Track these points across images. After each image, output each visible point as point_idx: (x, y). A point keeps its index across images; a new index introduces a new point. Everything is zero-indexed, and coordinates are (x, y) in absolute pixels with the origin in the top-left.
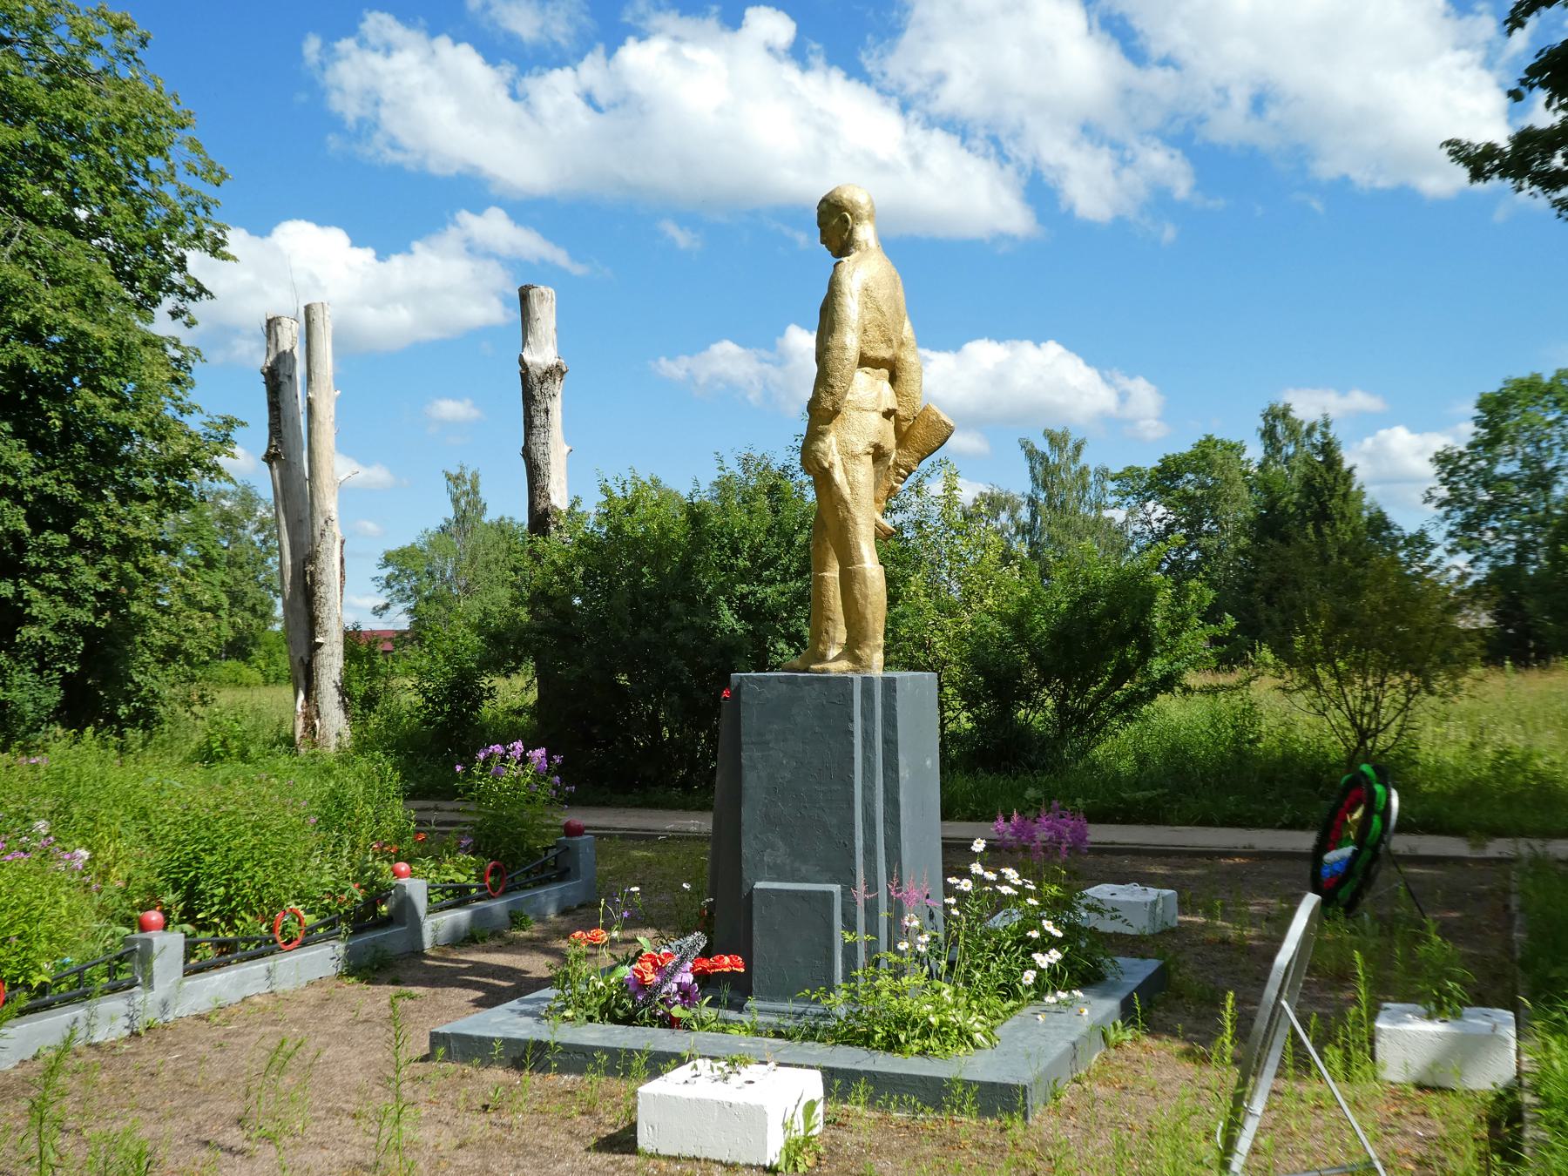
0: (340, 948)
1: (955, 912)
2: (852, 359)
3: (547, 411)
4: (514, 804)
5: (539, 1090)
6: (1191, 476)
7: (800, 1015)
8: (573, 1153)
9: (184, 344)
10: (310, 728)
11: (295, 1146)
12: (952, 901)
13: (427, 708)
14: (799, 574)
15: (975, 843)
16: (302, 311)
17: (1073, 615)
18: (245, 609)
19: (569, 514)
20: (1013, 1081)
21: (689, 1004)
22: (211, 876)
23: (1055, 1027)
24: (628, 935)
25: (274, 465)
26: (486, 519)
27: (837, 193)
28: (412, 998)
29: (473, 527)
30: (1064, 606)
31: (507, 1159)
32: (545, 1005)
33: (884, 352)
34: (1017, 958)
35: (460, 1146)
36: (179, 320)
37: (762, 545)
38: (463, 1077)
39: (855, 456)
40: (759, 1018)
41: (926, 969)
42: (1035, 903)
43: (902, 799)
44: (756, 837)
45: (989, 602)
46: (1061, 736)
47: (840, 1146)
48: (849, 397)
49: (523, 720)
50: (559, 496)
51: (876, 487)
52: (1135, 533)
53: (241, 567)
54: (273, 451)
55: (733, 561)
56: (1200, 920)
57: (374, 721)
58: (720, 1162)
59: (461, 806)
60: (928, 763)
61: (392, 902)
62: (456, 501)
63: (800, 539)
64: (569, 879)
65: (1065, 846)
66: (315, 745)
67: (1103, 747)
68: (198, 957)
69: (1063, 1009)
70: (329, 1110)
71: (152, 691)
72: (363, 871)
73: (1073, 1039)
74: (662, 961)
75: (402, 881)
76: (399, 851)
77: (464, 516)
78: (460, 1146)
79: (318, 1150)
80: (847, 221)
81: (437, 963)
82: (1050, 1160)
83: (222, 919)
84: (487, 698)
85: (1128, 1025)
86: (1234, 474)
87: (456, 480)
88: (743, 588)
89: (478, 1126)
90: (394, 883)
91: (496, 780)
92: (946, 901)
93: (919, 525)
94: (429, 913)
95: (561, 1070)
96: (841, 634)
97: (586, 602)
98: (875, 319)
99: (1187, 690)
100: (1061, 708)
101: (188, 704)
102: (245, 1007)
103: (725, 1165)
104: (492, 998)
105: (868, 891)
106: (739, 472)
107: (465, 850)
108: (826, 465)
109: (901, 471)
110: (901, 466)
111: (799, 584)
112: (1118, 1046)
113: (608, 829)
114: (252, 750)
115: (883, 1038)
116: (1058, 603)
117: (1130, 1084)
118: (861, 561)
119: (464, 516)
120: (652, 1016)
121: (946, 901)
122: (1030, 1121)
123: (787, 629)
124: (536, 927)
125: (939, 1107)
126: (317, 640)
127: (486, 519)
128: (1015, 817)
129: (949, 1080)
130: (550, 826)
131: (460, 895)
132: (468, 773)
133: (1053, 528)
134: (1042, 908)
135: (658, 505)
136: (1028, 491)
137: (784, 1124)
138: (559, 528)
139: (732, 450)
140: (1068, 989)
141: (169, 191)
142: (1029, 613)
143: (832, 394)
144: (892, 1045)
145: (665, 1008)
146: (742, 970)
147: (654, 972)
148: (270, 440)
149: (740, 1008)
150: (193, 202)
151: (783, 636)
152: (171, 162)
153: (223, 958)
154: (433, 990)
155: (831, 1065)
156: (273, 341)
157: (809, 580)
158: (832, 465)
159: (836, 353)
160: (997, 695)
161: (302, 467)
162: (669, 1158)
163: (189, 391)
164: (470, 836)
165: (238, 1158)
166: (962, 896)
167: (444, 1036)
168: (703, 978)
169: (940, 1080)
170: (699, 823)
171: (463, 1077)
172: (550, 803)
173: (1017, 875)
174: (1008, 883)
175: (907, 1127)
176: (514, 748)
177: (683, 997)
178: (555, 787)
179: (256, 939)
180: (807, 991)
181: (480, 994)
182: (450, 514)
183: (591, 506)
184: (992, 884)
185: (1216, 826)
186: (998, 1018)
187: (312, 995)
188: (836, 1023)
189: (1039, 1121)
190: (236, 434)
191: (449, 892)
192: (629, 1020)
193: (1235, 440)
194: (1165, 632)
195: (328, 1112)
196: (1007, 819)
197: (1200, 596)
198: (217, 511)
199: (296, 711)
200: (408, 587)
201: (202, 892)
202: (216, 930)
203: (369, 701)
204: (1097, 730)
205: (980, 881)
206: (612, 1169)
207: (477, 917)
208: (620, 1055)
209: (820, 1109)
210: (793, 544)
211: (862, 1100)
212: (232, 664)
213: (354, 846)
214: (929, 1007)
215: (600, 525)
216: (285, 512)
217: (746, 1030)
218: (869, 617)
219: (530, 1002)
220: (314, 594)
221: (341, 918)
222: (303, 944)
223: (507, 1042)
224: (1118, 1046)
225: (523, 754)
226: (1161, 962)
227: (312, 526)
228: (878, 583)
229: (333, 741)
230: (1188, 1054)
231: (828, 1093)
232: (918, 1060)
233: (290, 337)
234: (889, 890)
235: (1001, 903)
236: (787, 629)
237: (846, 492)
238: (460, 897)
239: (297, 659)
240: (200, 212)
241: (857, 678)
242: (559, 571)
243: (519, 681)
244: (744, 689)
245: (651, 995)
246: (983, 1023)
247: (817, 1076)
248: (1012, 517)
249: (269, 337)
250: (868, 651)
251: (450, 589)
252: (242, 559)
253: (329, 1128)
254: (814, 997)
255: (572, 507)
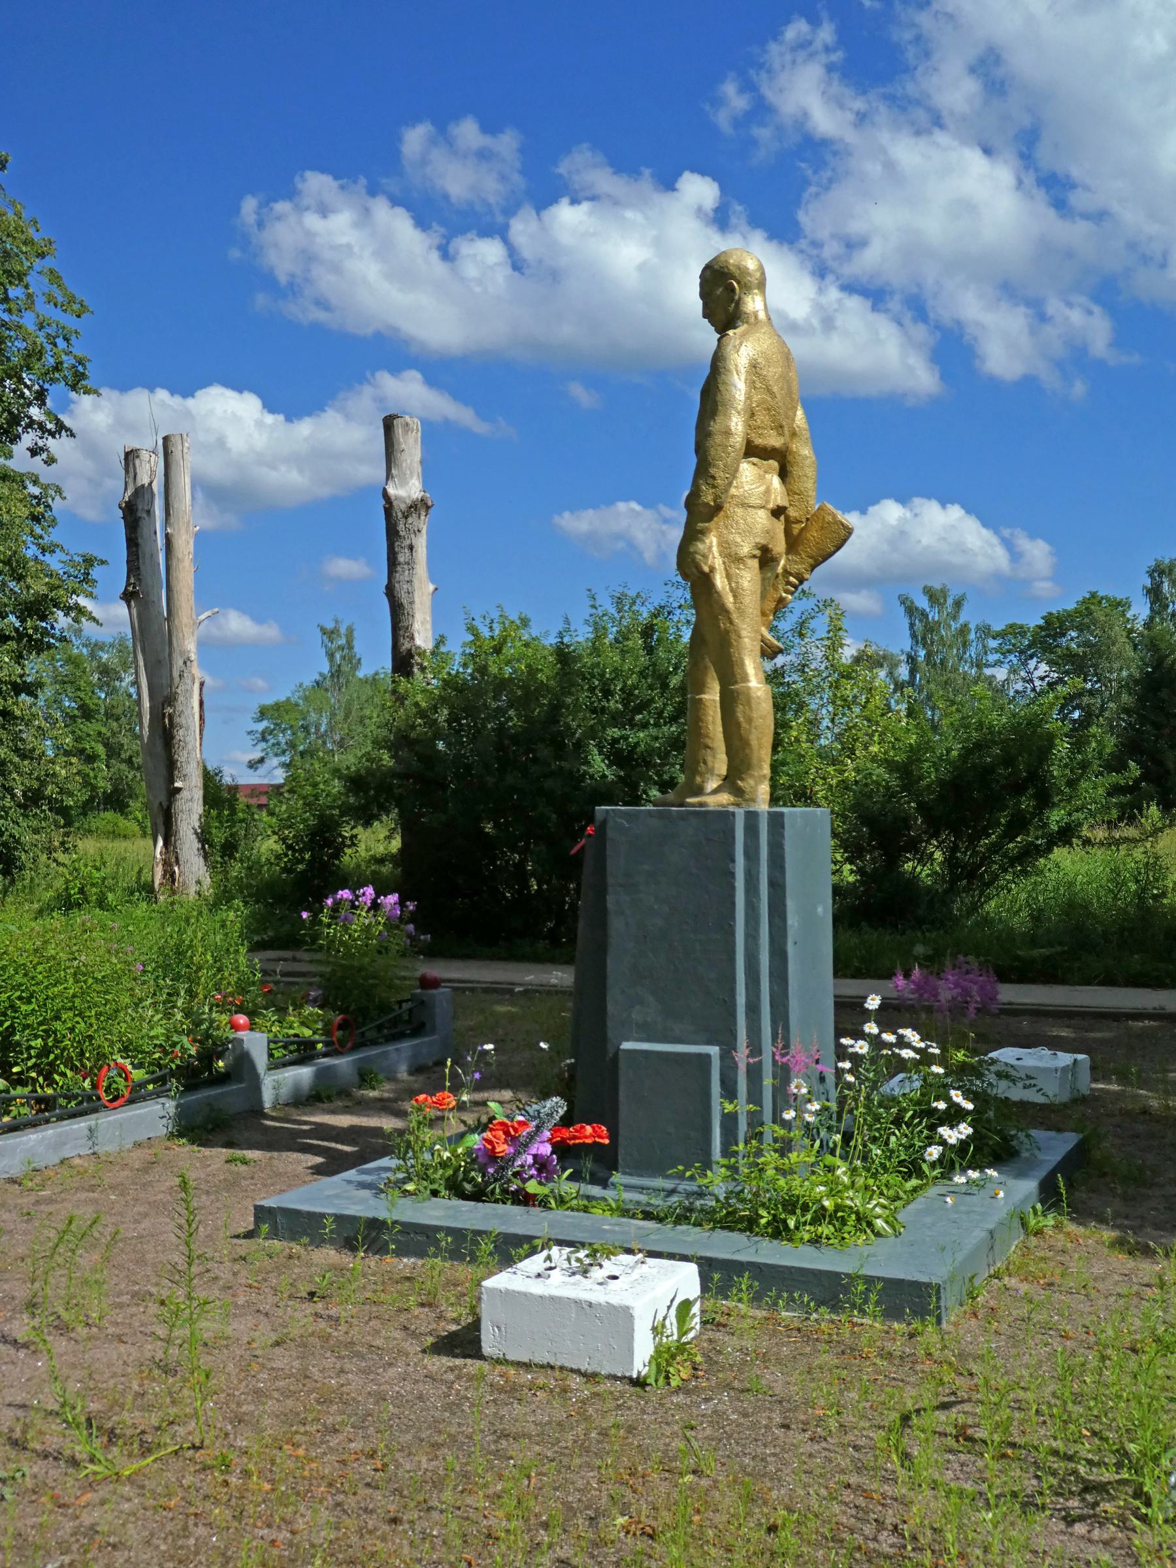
0: (170, 1106)
1: (850, 1078)
2: (738, 446)
3: (411, 548)
4: (365, 954)
5: (374, 1275)
6: (1074, 634)
7: (672, 1192)
8: (407, 1355)
9: (42, 480)
10: (169, 876)
11: (89, 1339)
12: (847, 1065)
13: (286, 855)
14: (673, 719)
15: (869, 1000)
16: (160, 442)
17: (965, 762)
18: (123, 761)
19: (433, 653)
20: (924, 1279)
21: (547, 1178)
22: (28, 1026)
23: (968, 1213)
24: (479, 1096)
25: (133, 603)
26: (360, 674)
27: (722, 259)
28: (245, 1162)
29: (348, 681)
30: (955, 753)
31: (330, 1362)
32: (384, 1175)
33: (774, 440)
34: (921, 1132)
35: (277, 1344)
36: (38, 458)
37: (635, 687)
38: (290, 1257)
39: (739, 560)
40: (627, 1196)
41: (818, 1143)
42: (941, 1071)
43: (791, 949)
44: (623, 992)
45: (874, 749)
46: (952, 890)
47: (720, 1352)
48: (733, 491)
49: (387, 869)
50: (423, 638)
51: (763, 596)
52: (1017, 692)
53: (117, 719)
54: (131, 589)
55: (604, 703)
56: (1115, 1087)
57: (236, 870)
58: (578, 1372)
59: (306, 956)
60: (820, 910)
61: (230, 1058)
62: (331, 656)
63: (674, 681)
64: (426, 1035)
65: (972, 1007)
66: (174, 893)
67: (993, 903)
68: (12, 1114)
69: (974, 1189)
70: (134, 1295)
71: (12, 836)
72: (198, 1024)
73: (991, 1226)
74: (516, 1130)
75: (241, 1034)
76: (242, 1002)
77: (339, 671)
78: (277, 1344)
79: (115, 1343)
80: (733, 290)
81: (277, 1124)
82: (971, 1374)
83: (39, 1073)
84: (349, 847)
85: (1049, 1209)
86: (1118, 631)
87: (330, 634)
88: (613, 732)
89: (301, 1317)
90: (231, 1036)
91: (346, 929)
92: (840, 1065)
93: (802, 669)
94: (270, 1069)
95: (399, 1253)
96: (721, 765)
97: (448, 745)
98: (763, 401)
99: (1087, 842)
100: (951, 862)
101: (50, 850)
102: (65, 1172)
103: (584, 1375)
104: (333, 1165)
105: (752, 1054)
106: (612, 610)
107: (314, 1002)
108: (706, 569)
109: (792, 579)
110: (791, 574)
111: (673, 729)
112: (1039, 1233)
113: (471, 982)
114: (110, 896)
115: (768, 1223)
116: (949, 750)
117: (1058, 1281)
118: (745, 679)
119: (339, 671)
120: (505, 1191)
121: (840, 1065)
122: (944, 1325)
123: (660, 776)
124: (387, 1086)
125: (835, 1307)
126: (176, 785)
127: (360, 674)
128: (917, 972)
129: (848, 1275)
130: (405, 978)
131: (305, 1050)
132: (315, 921)
133: (932, 686)
134: (946, 1075)
135: (527, 645)
136: (908, 649)
137: (654, 1329)
138: (423, 669)
139: (607, 588)
140: (980, 1167)
141: (28, 321)
142: (919, 760)
143: (714, 487)
144: (779, 1231)
145: (519, 1182)
146: (607, 1141)
147: (506, 1142)
148: (128, 578)
149: (604, 1183)
150: (54, 334)
151: (656, 783)
152: (30, 291)
153: (41, 1116)
154: (268, 1154)
155: (708, 1254)
156: (131, 474)
157: (684, 724)
158: (712, 569)
159: (718, 439)
160: (880, 846)
161: (161, 606)
162: (519, 1364)
163: (51, 529)
164: (319, 987)
165: (22, 1354)
166: (856, 1059)
167: (270, 1211)
168: (563, 1150)
169: (838, 1274)
170: (561, 977)
171: (290, 1257)
172: (403, 954)
173: (918, 1037)
174: (909, 1046)
175: (799, 1330)
176: (364, 894)
177: (540, 1171)
178: (409, 936)
179: (77, 1096)
180: (681, 1168)
181: (319, 1160)
182: (326, 668)
183: (457, 646)
184: (890, 1046)
185: (1119, 986)
186: (899, 1198)
187: (137, 1158)
188: (713, 1204)
189: (956, 1324)
190: (96, 572)
191: (292, 1048)
192: (479, 1195)
193: (1120, 596)
194: (1063, 781)
195: (133, 1297)
196: (907, 975)
197: (1099, 743)
198: (95, 664)
199: (155, 857)
200: (284, 741)
201: (18, 1044)
202: (34, 1085)
203: (229, 848)
204: (988, 885)
205: (876, 1043)
206: (451, 1377)
207: (322, 1075)
208: (465, 1236)
209: (696, 1309)
210: (667, 685)
211: (745, 1298)
212: (109, 815)
213: (191, 994)
214: (822, 1188)
215: (465, 666)
216: (143, 651)
217: (611, 1209)
218: (754, 743)
219: (368, 1172)
220: (172, 737)
221: (172, 1074)
222: (131, 1101)
223: (340, 1219)
224: (1039, 1233)
225: (374, 902)
226: (1081, 1136)
227: (171, 671)
228: (764, 705)
229: (193, 889)
230: (1119, 1244)
231: (705, 1288)
232: (810, 1250)
233: (149, 470)
234: (774, 1054)
235: (901, 1065)
236: (660, 776)
237: (729, 600)
238: (303, 1052)
239: (156, 804)
240: (60, 341)
241: (740, 813)
242: (422, 713)
243: (380, 829)
244: (610, 824)
245: (503, 1168)
246: (884, 1207)
247: (692, 1268)
248: (891, 674)
249: (127, 471)
250: (752, 782)
251: (324, 743)
252: (119, 711)
253: (132, 1316)
254: (688, 1174)
255: (437, 646)
